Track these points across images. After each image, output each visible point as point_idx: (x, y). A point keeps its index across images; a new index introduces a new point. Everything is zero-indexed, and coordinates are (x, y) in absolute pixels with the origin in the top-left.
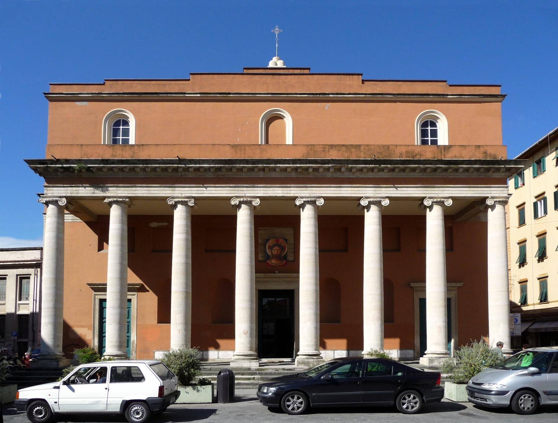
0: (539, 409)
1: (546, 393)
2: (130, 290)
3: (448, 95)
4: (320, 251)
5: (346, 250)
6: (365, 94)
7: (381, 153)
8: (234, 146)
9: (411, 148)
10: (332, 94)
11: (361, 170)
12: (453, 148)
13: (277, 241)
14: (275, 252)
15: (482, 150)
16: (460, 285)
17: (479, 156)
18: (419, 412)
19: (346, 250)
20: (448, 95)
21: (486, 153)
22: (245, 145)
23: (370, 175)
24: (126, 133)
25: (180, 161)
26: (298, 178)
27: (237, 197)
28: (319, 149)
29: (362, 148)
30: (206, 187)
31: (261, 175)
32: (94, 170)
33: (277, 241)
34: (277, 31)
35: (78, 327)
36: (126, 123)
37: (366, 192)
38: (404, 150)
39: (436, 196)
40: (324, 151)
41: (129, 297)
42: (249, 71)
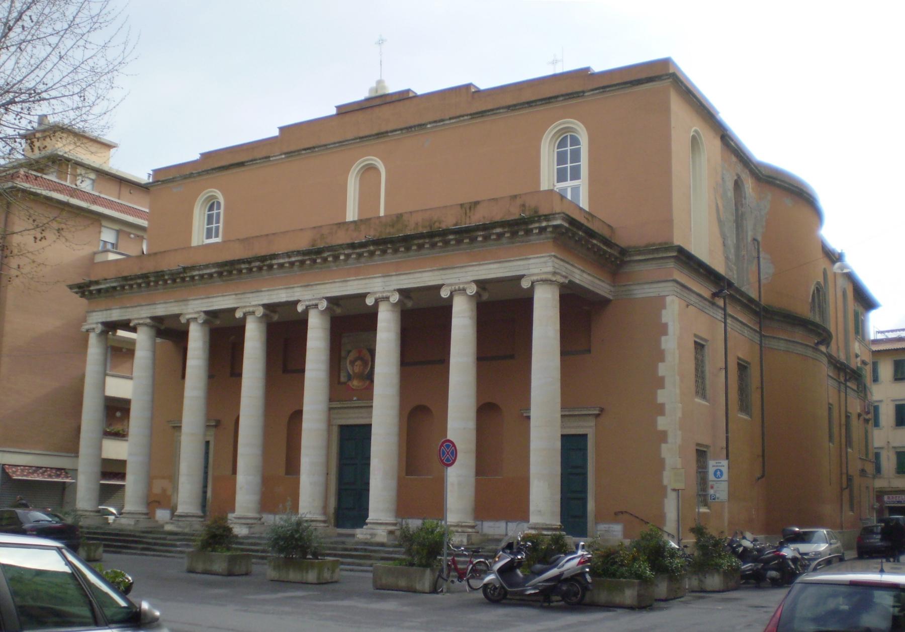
14: (357, 369)
15: (519, 202)
17: (515, 213)
21: (524, 205)
39: (457, 281)
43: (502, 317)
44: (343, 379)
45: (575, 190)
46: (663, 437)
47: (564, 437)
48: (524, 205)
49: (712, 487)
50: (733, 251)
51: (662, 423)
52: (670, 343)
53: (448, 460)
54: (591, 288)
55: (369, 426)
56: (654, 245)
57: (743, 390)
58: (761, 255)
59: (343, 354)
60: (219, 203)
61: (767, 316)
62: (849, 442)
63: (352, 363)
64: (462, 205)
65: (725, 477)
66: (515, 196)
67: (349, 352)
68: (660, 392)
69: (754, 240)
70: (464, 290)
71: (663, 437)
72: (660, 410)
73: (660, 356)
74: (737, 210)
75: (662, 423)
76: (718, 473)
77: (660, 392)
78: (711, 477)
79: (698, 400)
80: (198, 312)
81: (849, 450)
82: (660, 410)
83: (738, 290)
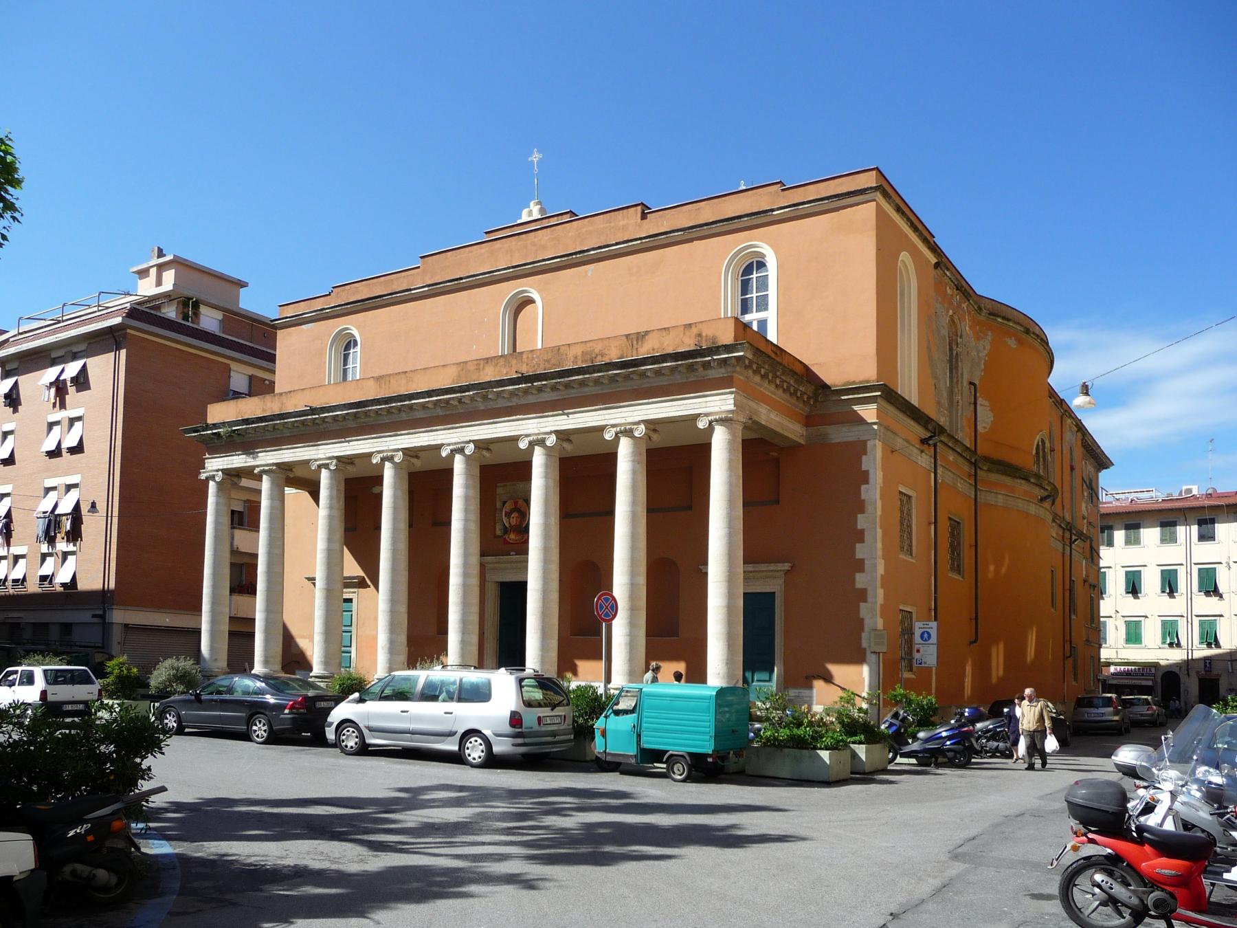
0: (364, 750)
1: (370, 729)
2: (347, 585)
3: (773, 210)
4: (651, 510)
5: (777, 502)
6: (640, 239)
7: (548, 361)
8: (379, 379)
9: (589, 345)
10: (593, 249)
11: (512, 393)
12: (650, 335)
13: (516, 503)
14: (513, 522)
15: (694, 331)
16: (787, 566)
17: (688, 345)
18: (684, 781)
19: (777, 502)
20: (773, 210)
21: (700, 335)
22: (389, 375)
23: (531, 399)
24: (763, 284)
25: (313, 411)
26: (446, 416)
27: (379, 452)
28: (471, 367)
29: (525, 356)
30: (568, 414)
31: (404, 416)
32: (430, 405)
33: (516, 503)
34: (536, 157)
35: (303, 637)
36: (761, 265)
37: (445, 437)
38: (577, 351)
39: (623, 421)
40: (478, 369)
41: (346, 596)
42: (494, 236)
43: (676, 466)
44: (498, 533)
45: (763, 323)
46: (862, 595)
47: (747, 596)
48: (700, 335)
49: (918, 651)
50: (945, 395)
51: (861, 580)
52: (873, 493)
53: (607, 615)
54: (781, 431)
55: (525, 584)
56: (854, 383)
57: (955, 548)
58: (980, 401)
59: (499, 505)
60: (355, 342)
61: (986, 463)
62: (1072, 608)
63: (508, 515)
64: (627, 336)
65: (934, 639)
66: (690, 325)
67: (504, 503)
68: (858, 546)
69: (971, 383)
70: (631, 431)
71: (862, 595)
72: (860, 566)
73: (860, 507)
74: (951, 349)
75: (861, 580)
76: (925, 636)
77: (858, 546)
78: (917, 639)
79: (902, 556)
80: (330, 458)
81: (1073, 617)
82: (860, 566)
83: (951, 437)
